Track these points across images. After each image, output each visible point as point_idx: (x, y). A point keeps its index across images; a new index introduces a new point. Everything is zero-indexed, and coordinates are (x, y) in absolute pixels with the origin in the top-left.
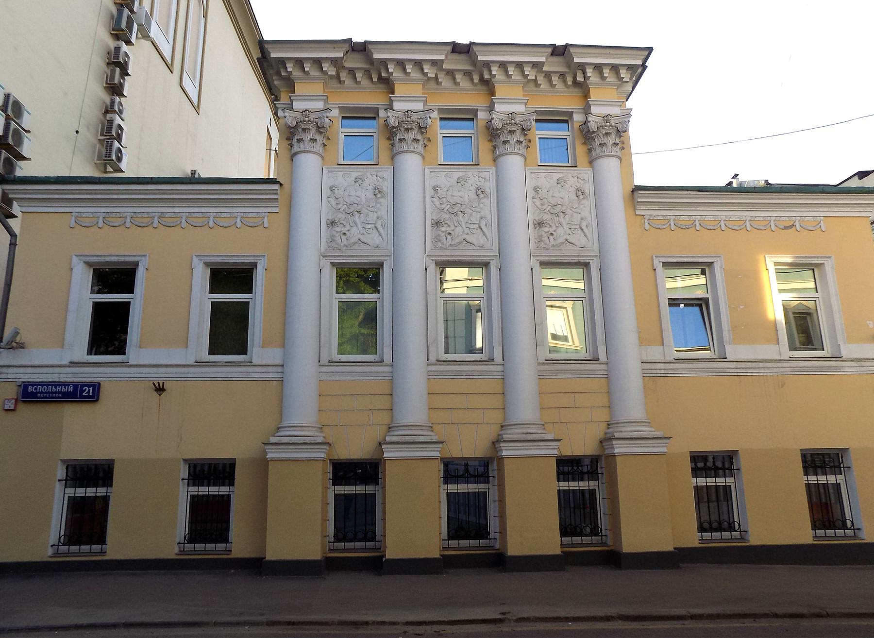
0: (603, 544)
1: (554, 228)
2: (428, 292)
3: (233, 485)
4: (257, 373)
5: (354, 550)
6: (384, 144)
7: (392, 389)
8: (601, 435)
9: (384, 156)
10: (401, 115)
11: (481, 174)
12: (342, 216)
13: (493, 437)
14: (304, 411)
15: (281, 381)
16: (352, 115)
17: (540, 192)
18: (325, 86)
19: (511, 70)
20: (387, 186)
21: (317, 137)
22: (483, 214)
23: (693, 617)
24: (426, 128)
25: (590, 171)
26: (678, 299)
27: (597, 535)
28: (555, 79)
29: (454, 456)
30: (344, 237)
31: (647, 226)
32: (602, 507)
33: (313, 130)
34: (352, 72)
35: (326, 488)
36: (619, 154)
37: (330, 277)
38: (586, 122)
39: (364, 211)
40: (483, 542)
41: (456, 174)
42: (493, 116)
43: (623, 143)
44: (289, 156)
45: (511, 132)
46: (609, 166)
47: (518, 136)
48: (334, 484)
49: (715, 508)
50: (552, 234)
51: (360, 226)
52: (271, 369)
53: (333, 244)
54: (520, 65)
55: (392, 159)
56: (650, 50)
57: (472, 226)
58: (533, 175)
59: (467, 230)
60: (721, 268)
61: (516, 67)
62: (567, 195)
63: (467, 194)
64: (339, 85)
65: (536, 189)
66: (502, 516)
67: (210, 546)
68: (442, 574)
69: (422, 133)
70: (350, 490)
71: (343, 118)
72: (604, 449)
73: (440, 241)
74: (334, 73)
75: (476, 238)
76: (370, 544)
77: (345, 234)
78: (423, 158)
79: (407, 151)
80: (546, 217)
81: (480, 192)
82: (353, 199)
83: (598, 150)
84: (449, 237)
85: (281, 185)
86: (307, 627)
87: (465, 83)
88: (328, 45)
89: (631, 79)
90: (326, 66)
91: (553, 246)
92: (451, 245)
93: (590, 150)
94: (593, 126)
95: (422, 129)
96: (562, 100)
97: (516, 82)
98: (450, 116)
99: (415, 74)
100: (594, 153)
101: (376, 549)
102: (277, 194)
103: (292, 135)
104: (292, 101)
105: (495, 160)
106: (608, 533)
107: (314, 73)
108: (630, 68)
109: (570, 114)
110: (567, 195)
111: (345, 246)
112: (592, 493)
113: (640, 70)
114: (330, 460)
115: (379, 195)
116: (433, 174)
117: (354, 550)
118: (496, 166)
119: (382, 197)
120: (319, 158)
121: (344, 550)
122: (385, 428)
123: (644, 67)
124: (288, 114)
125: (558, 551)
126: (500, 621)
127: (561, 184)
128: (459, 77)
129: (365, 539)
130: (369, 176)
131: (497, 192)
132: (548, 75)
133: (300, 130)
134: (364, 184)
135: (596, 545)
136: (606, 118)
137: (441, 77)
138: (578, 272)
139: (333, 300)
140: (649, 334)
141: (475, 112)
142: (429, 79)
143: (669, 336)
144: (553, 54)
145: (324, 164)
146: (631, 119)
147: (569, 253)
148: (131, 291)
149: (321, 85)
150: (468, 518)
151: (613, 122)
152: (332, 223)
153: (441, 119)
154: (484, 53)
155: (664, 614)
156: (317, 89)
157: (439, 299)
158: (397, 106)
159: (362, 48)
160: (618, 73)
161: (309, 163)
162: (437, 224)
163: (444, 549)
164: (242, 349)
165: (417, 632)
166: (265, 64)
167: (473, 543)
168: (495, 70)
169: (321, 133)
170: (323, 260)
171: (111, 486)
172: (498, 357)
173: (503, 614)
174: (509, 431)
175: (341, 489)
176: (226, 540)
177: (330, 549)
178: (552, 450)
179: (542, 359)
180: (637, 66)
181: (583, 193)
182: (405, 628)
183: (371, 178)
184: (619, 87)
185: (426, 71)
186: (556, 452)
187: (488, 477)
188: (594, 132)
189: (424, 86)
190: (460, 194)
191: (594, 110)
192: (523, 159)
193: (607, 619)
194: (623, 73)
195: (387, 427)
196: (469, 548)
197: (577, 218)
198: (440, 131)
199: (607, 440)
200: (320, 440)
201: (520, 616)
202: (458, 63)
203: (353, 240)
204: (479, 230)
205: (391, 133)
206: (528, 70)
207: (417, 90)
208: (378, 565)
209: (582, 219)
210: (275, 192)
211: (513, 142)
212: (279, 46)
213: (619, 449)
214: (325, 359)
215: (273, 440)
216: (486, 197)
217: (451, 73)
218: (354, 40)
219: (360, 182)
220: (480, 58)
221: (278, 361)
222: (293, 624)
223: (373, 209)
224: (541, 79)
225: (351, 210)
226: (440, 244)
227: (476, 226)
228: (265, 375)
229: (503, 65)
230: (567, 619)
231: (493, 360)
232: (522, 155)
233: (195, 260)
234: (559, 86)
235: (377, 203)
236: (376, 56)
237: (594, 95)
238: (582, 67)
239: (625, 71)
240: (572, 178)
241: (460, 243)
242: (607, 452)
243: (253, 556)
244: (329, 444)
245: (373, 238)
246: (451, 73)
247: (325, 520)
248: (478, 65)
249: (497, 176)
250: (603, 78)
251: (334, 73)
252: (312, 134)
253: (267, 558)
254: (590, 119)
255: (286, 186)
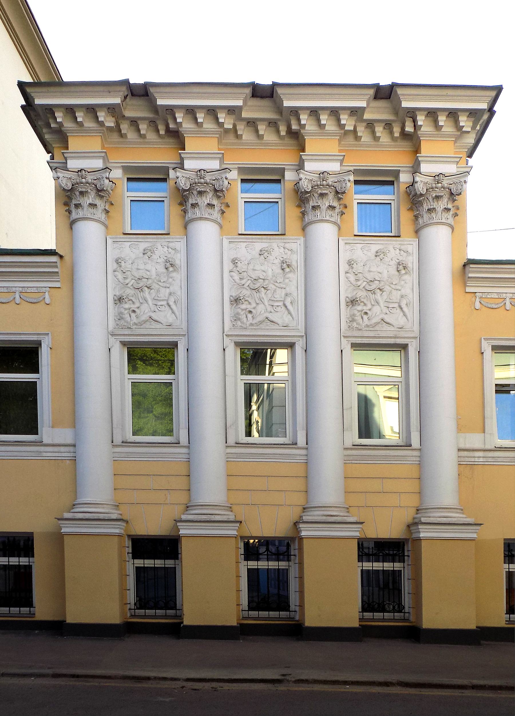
0: (404, 620)
1: (369, 306)
2: (340, 377)
3: (33, 556)
4: (48, 453)
5: (155, 617)
6: (176, 210)
7: (189, 470)
8: (410, 520)
9: (176, 223)
10: (193, 175)
11: (287, 245)
12: (130, 292)
13: (295, 518)
14: (98, 488)
15: (74, 460)
16: (138, 176)
17: (355, 266)
18: (104, 140)
19: (324, 118)
20: (180, 259)
21: (98, 202)
22: (403, 292)
23: (474, 687)
24: (344, 193)
25: (301, 240)
26: (508, 385)
27: (400, 611)
28: (379, 130)
29: (369, 536)
30: (133, 315)
31: (478, 305)
32: (407, 587)
33: (93, 194)
34: (134, 123)
35: (122, 562)
36: (451, 221)
37: (120, 357)
38: (414, 183)
39: (155, 286)
40: (283, 614)
41: (259, 245)
42: (301, 176)
43: (458, 209)
44: (68, 226)
45: (322, 195)
46: (438, 236)
47: (330, 200)
48: (134, 557)
49: (269, 591)
50: (366, 313)
51: (382, 306)
52: (62, 449)
53: (122, 322)
54: (335, 112)
55: (186, 227)
56: (499, 89)
57: (391, 305)
58: (348, 247)
59: (385, 310)
60: (48, 346)
61: (330, 115)
62: (386, 270)
63: (270, 269)
64: (121, 140)
65: (350, 263)
66: (301, 592)
67: (15, 610)
68: (239, 640)
69: (219, 197)
70: (149, 563)
71: (129, 179)
72: (412, 533)
73: (239, 319)
74: (231, 127)
75: (280, 317)
76: (170, 612)
77: (134, 311)
78: (221, 227)
79: (201, 219)
80: (361, 294)
81: (286, 266)
82: (142, 273)
83: (426, 216)
84: (250, 316)
85: (61, 257)
86: (91, 680)
87: (270, 137)
88: (101, 88)
89: (473, 128)
90: (102, 116)
91: (367, 326)
92: (251, 324)
93: (416, 217)
94: (420, 188)
95: (218, 192)
96: (386, 156)
97: (329, 134)
98: (253, 178)
99: (209, 125)
100: (420, 221)
101: (176, 616)
102: (56, 267)
103: (68, 198)
104: (66, 159)
105: (304, 229)
106: (411, 610)
107: (89, 124)
108: (473, 114)
109: (396, 174)
110: (386, 270)
111: (135, 324)
112: (286, 572)
113: (485, 117)
114: (129, 536)
115: (171, 269)
116: (232, 245)
117: (155, 617)
118: (305, 236)
119: (175, 271)
120: (103, 228)
121: (145, 616)
122: (183, 507)
123: (491, 112)
124: (180, 173)
125: (356, 624)
126: (278, 681)
127: (379, 257)
128: (262, 128)
129: (166, 608)
130: (160, 247)
131: (305, 265)
132: (370, 125)
133: (77, 193)
134: (154, 257)
135: (171, 617)
136: (438, 177)
137: (241, 128)
138: (395, 357)
139: (124, 380)
140: (470, 420)
141: (282, 171)
142: (227, 131)
143: (492, 424)
144: (254, 95)
145: (339, 235)
146: (470, 179)
147: (386, 335)
148: (35, 369)
149: (99, 140)
150: (269, 591)
151: (446, 182)
152: (119, 300)
153: (243, 181)
154: (414, 98)
155: (444, 683)
156: (94, 144)
157: (239, 380)
158: (188, 164)
159: (142, 92)
160: (456, 121)
161: (91, 233)
162: (236, 301)
163: (244, 618)
164: (33, 429)
165: (195, 687)
166: (32, 114)
167: (273, 614)
168: (304, 118)
169: (102, 197)
170: (112, 339)
171: (33, 556)
172: (301, 441)
173: (283, 675)
174: (312, 513)
175: (139, 563)
176: (29, 604)
177: (132, 615)
178: (355, 532)
179: (348, 443)
180: (482, 111)
181: (405, 268)
182: (185, 684)
183: (161, 249)
184: (457, 138)
185: (221, 120)
186: (357, 534)
187: (404, 556)
188: (421, 195)
189: (220, 142)
190: (263, 268)
191: (425, 168)
192: (451, 230)
193: (387, 684)
194: (464, 121)
195: (301, 508)
196: (269, 618)
197: (396, 296)
198: (240, 196)
199: (413, 525)
200: (114, 516)
201: (298, 678)
202: (135, 110)
203: (144, 318)
204: (283, 308)
205: (301, 198)
206: (344, 119)
207: (211, 145)
208: (177, 630)
209: (402, 297)
210: (54, 265)
211: (324, 207)
212: (90, 89)
213: (424, 533)
214: (118, 440)
215: (67, 515)
216: (292, 271)
217: (252, 123)
218: (131, 82)
219: (149, 254)
220: (286, 104)
221: (69, 441)
222: (78, 676)
223: (165, 285)
224: (361, 130)
225: (140, 285)
226: (239, 323)
227: (164, 303)
228: (57, 454)
229: (314, 112)
230: (345, 683)
231: (296, 444)
232: (335, 223)
233: (484, 344)
234: (385, 138)
235: (169, 277)
236: (160, 102)
237: (426, 148)
238: (412, 113)
239: (346, 117)
240: (393, 249)
241: (261, 322)
242: (414, 536)
243: (56, 619)
244: (127, 522)
245: (165, 316)
246: (252, 123)
247: (123, 590)
248: (401, 113)
249: (306, 247)
250: (437, 127)
251: (112, 125)
252: (91, 198)
253: (67, 622)
254: (417, 179)
255: (67, 258)
